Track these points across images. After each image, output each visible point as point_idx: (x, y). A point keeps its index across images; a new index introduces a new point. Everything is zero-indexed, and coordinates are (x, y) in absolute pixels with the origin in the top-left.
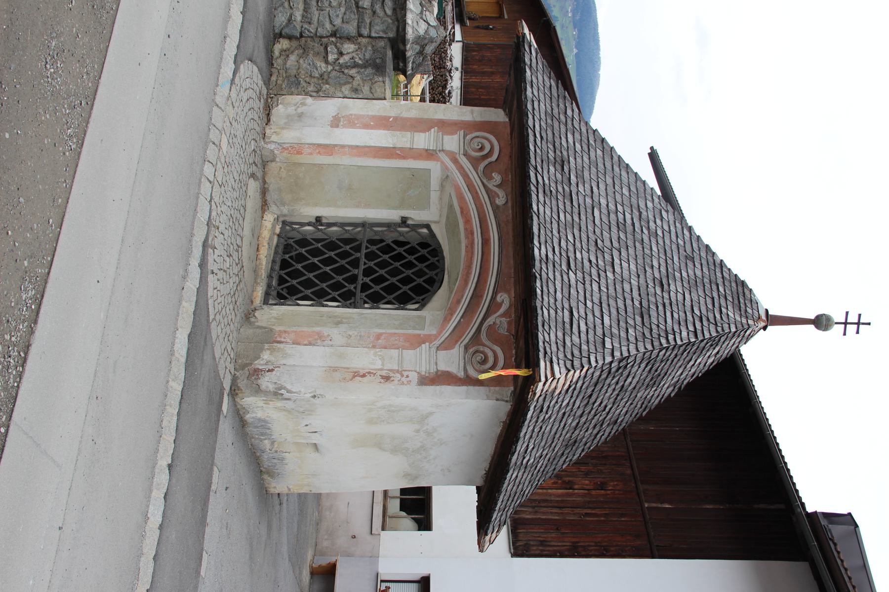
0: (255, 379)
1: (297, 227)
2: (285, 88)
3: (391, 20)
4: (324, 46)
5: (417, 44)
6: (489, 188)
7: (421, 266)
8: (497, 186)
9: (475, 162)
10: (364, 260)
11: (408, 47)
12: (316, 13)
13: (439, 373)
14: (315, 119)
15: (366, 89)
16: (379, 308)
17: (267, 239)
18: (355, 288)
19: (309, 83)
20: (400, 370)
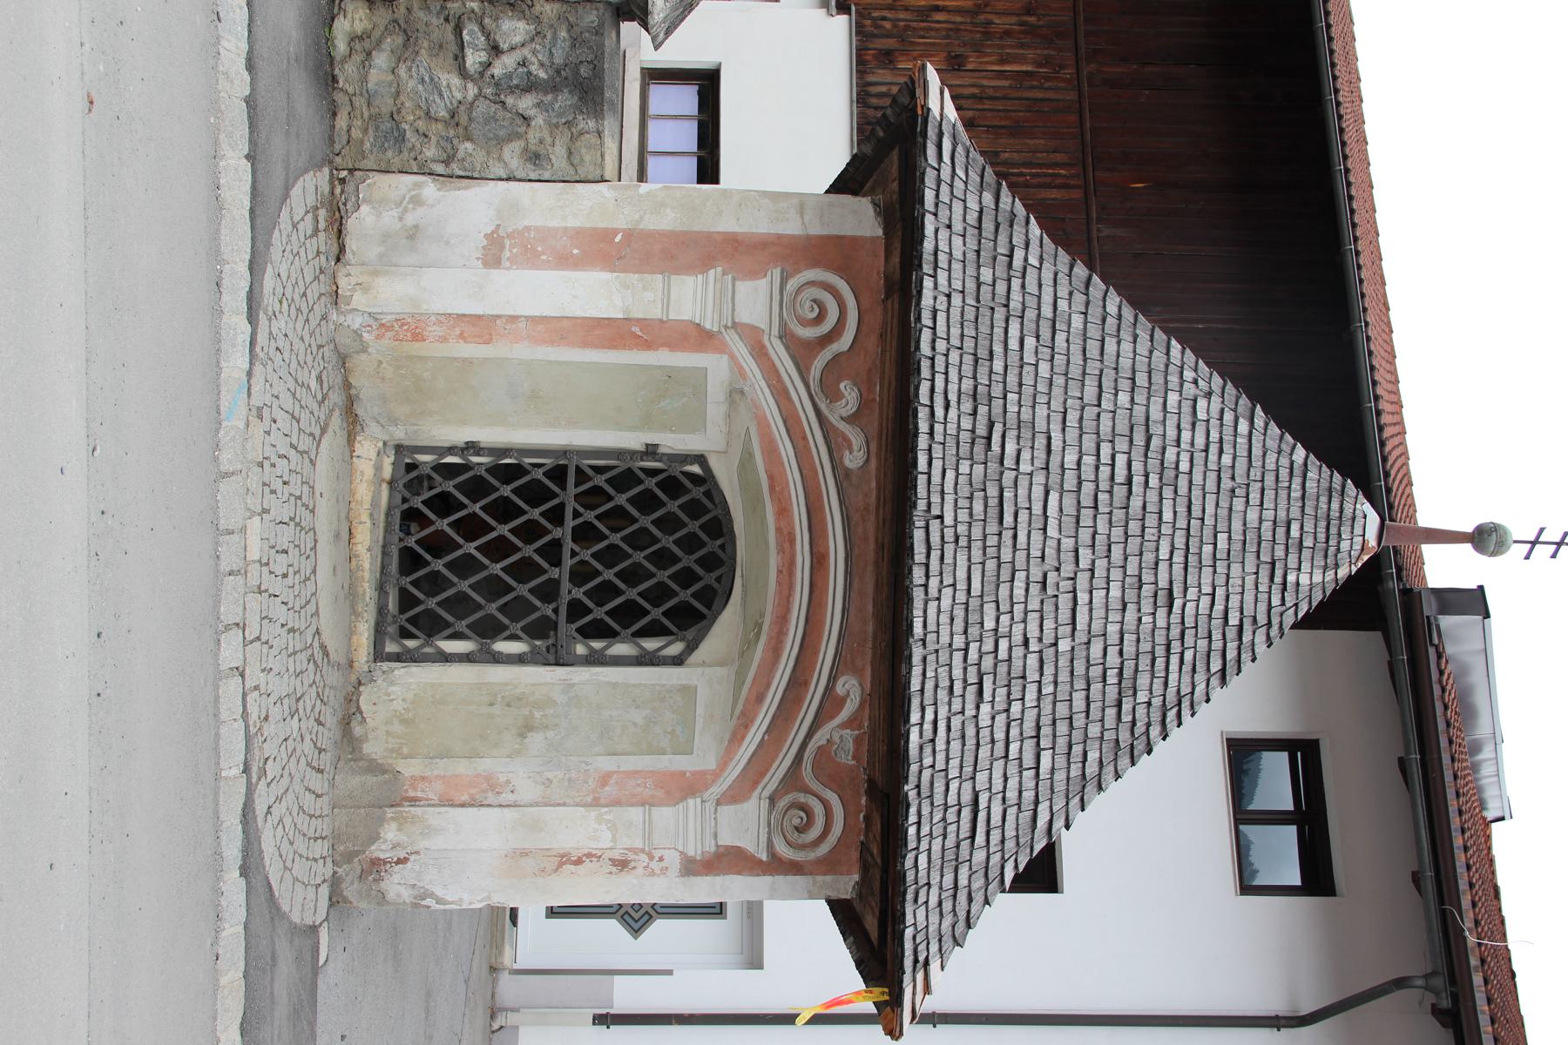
0: (374, 880)
4: (452, 24)
9: (802, 352)
13: (722, 850)
14: (447, 243)
15: (558, 154)
17: (367, 505)
18: (556, 611)
19: (426, 136)
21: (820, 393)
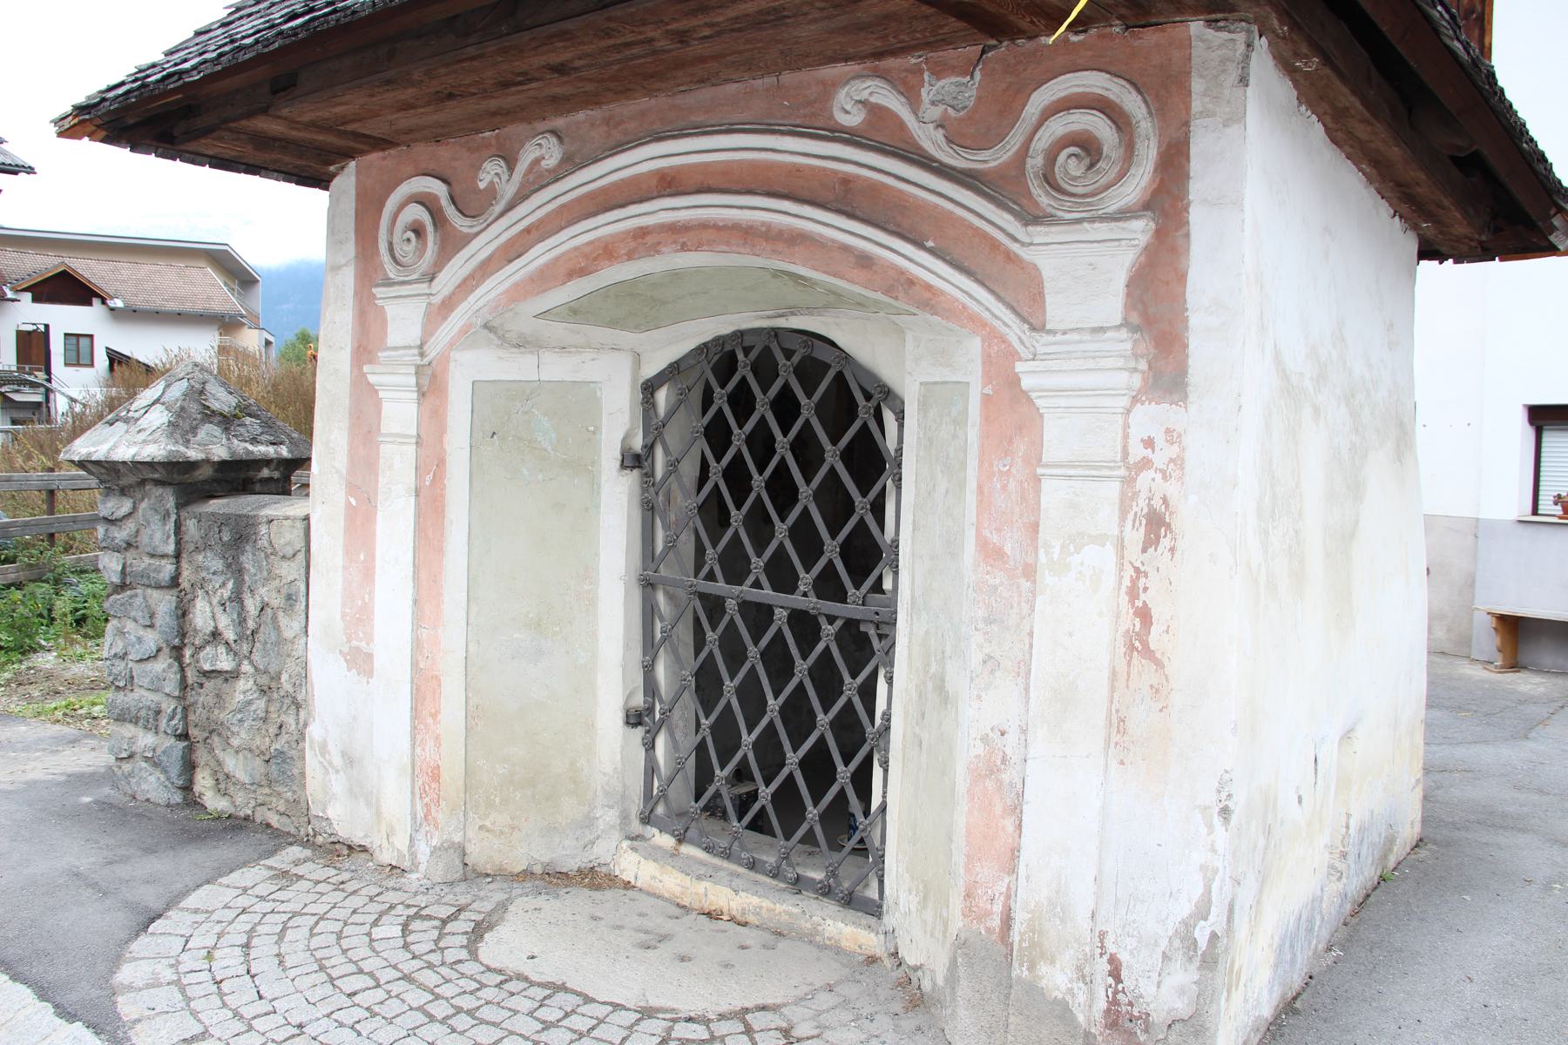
0: (1146, 1031)
1: (656, 784)
2: (294, 792)
3: (143, 499)
4: (204, 680)
5: (194, 430)
6: (516, 194)
7: (763, 407)
8: (511, 169)
9: (451, 244)
10: (744, 588)
11: (194, 454)
12: (139, 693)
13: (1135, 318)
16: (895, 544)
18: (831, 619)
19: (281, 727)
20: (1122, 472)
21: (484, 217)
